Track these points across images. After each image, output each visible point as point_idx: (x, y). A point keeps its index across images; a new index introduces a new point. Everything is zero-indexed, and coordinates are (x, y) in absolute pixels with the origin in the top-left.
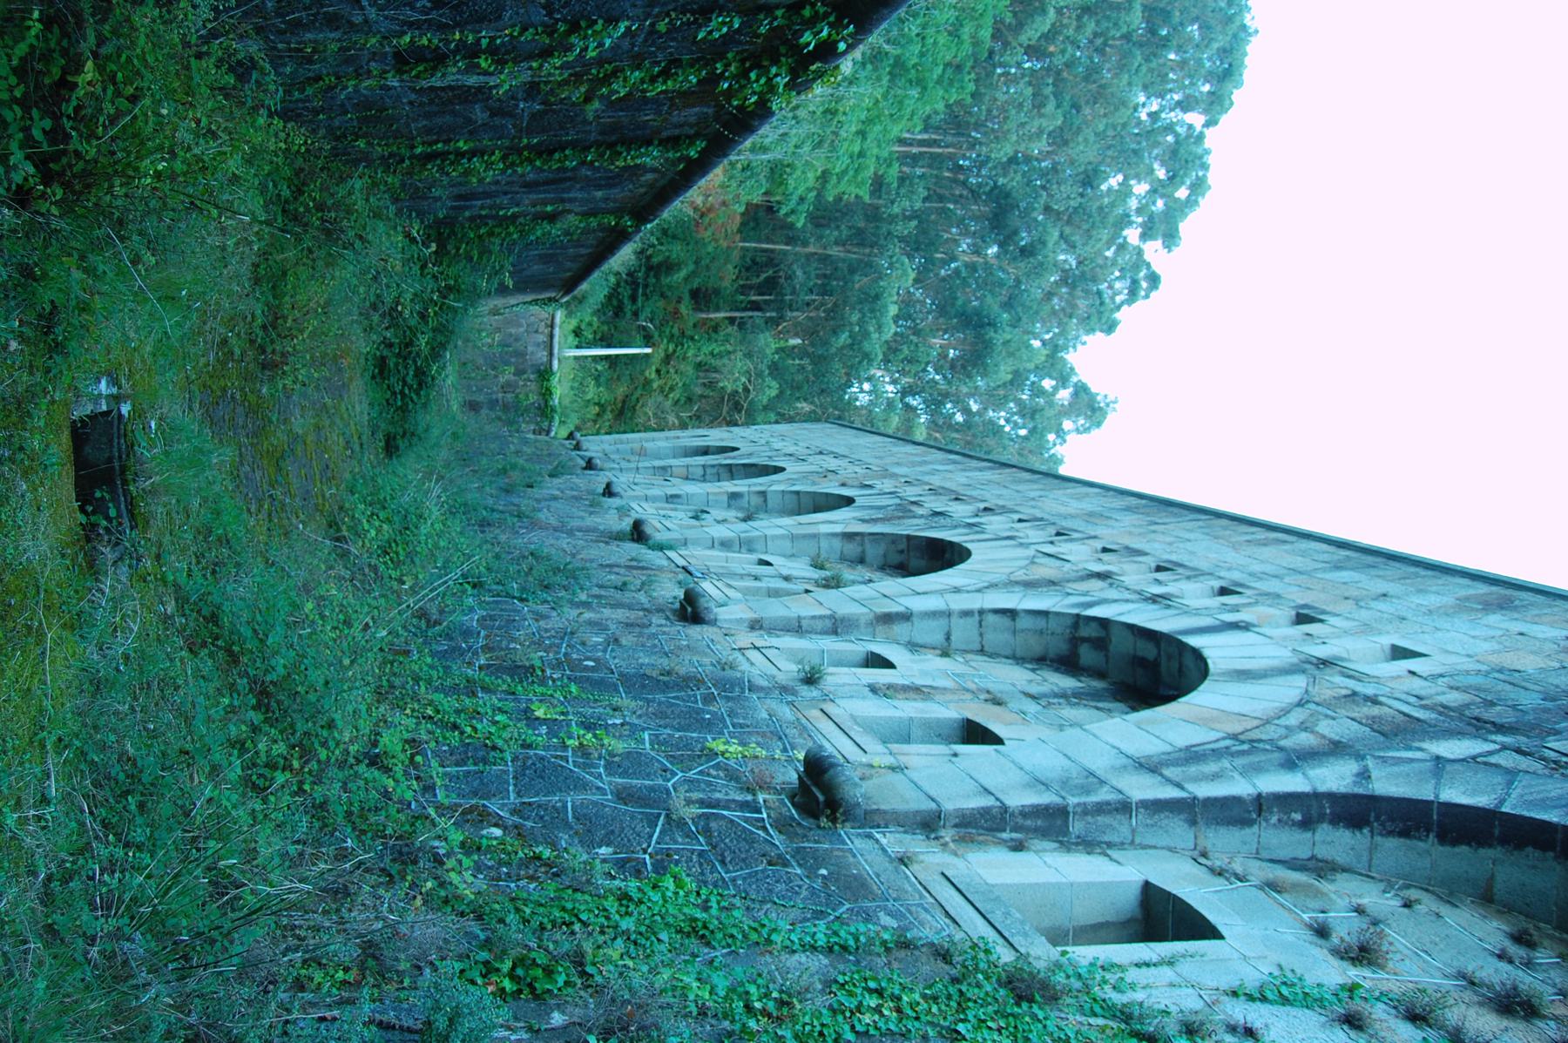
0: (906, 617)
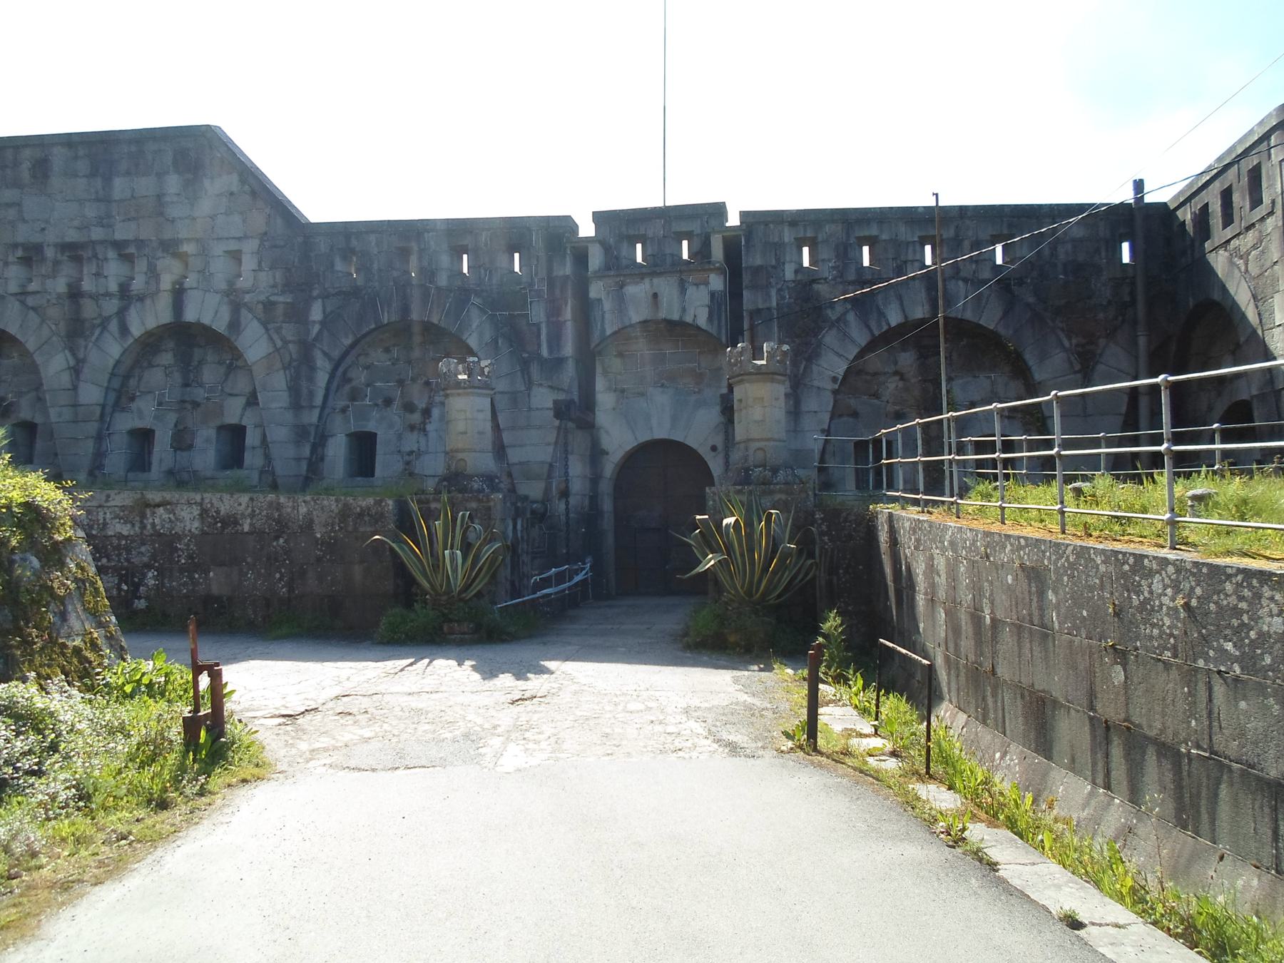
0: (103, 406)
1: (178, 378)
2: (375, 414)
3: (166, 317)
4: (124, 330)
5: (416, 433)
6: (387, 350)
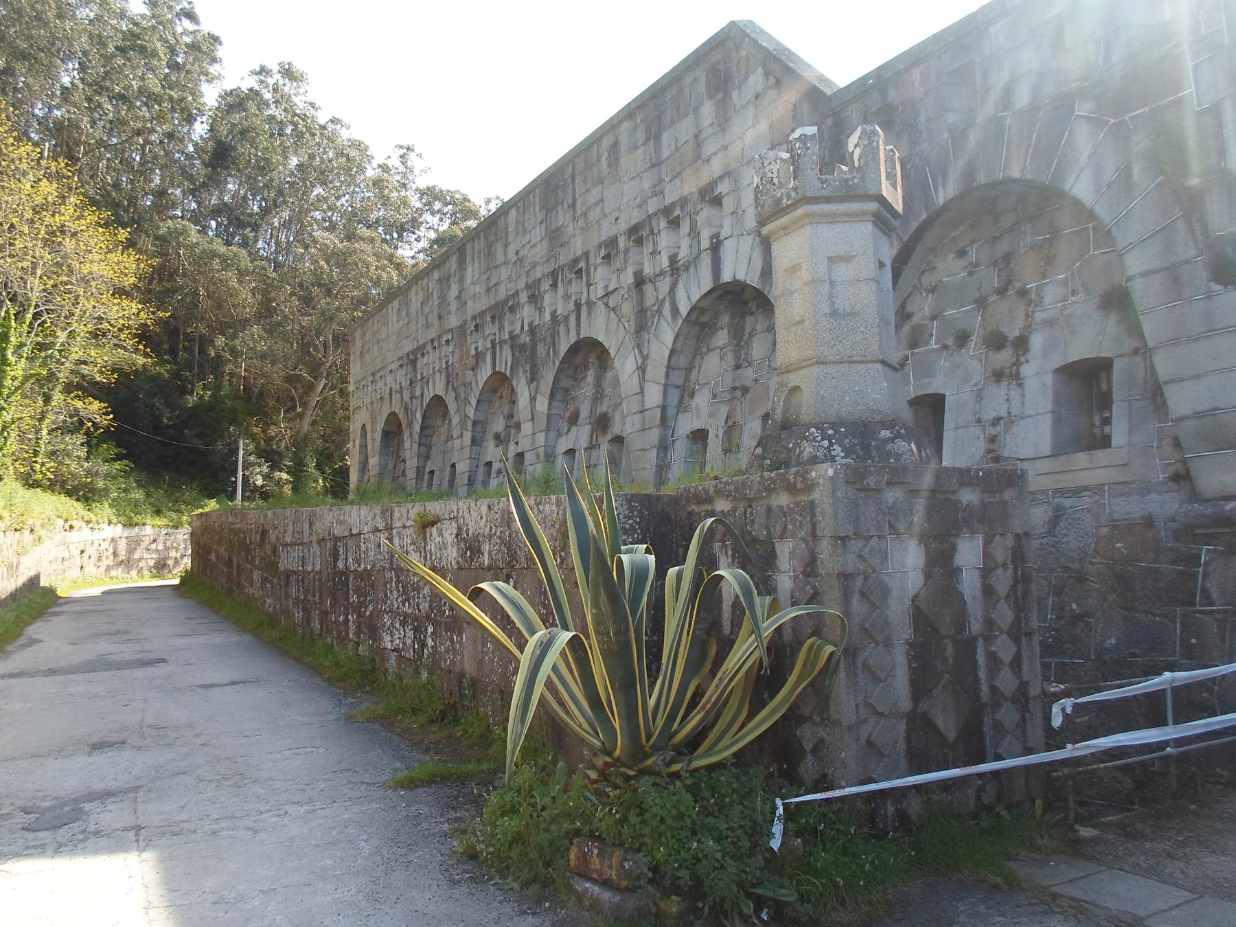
0: (664, 408)
1: (730, 358)
2: (943, 363)
3: (707, 284)
4: (675, 311)
5: (1004, 384)
6: (962, 254)
